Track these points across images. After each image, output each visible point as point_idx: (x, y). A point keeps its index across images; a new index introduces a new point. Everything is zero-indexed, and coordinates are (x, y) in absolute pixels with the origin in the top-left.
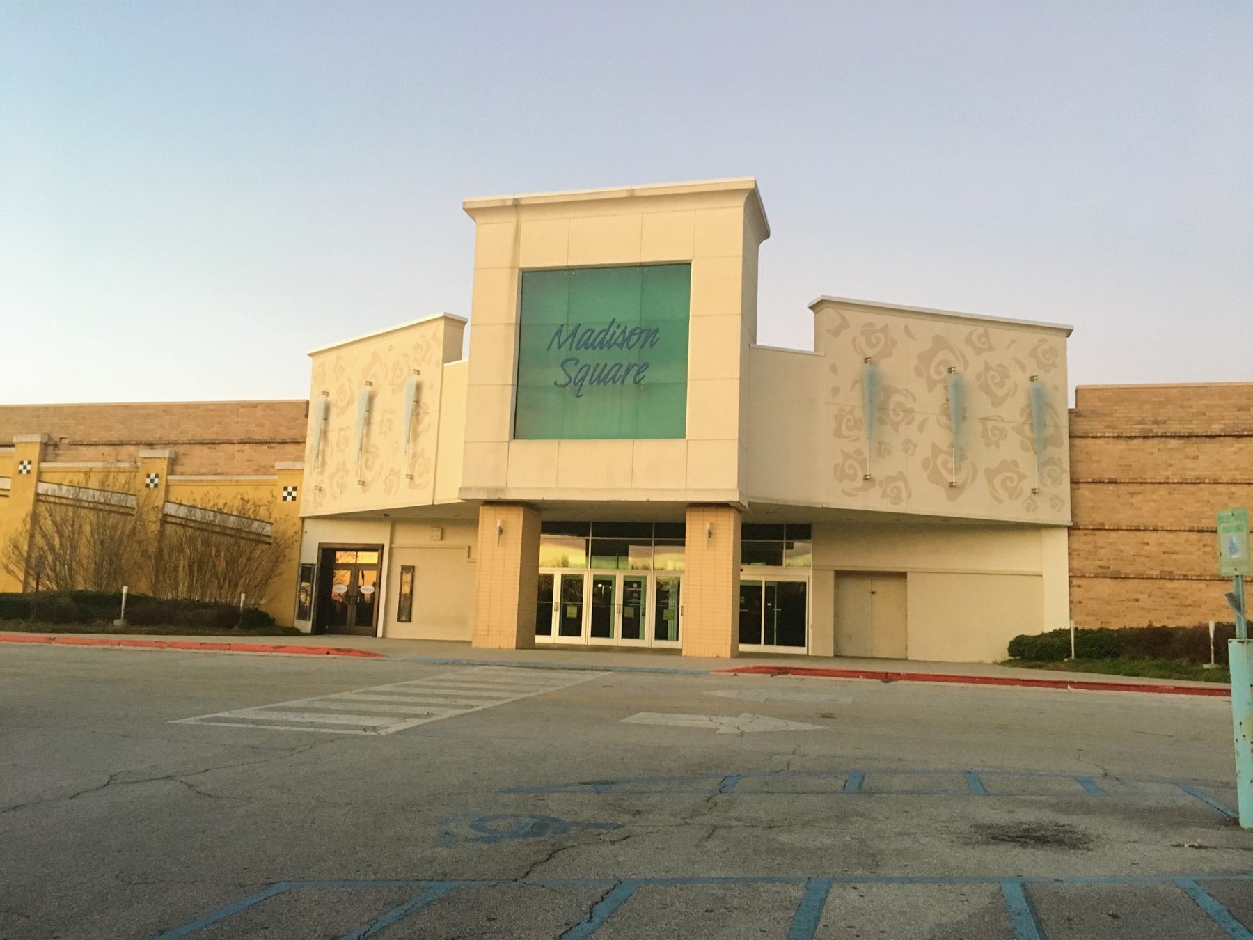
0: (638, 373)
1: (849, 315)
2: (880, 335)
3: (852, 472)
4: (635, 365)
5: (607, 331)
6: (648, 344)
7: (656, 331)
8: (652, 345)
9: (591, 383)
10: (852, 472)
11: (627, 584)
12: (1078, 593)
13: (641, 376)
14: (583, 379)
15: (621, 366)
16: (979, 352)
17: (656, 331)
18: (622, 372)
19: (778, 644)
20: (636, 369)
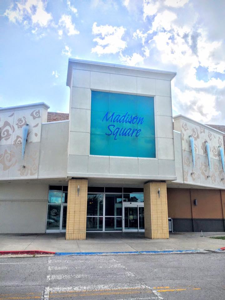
0: (137, 133)
1: (189, 124)
2: (38, 116)
3: (6, 133)
4: (136, 130)
5: (125, 117)
6: (140, 123)
7: (143, 119)
8: (141, 123)
9: (120, 135)
10: (6, 133)
11: (121, 226)
12: (142, 208)
13: (138, 134)
14: (117, 132)
15: (131, 129)
16: (34, 118)
17: (143, 119)
18: (132, 131)
19: (102, 228)
20: (136, 132)
